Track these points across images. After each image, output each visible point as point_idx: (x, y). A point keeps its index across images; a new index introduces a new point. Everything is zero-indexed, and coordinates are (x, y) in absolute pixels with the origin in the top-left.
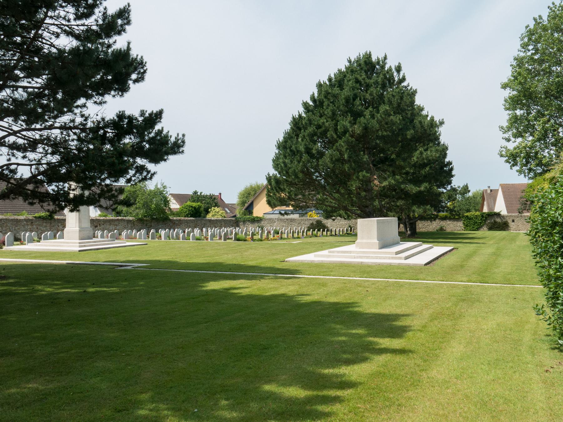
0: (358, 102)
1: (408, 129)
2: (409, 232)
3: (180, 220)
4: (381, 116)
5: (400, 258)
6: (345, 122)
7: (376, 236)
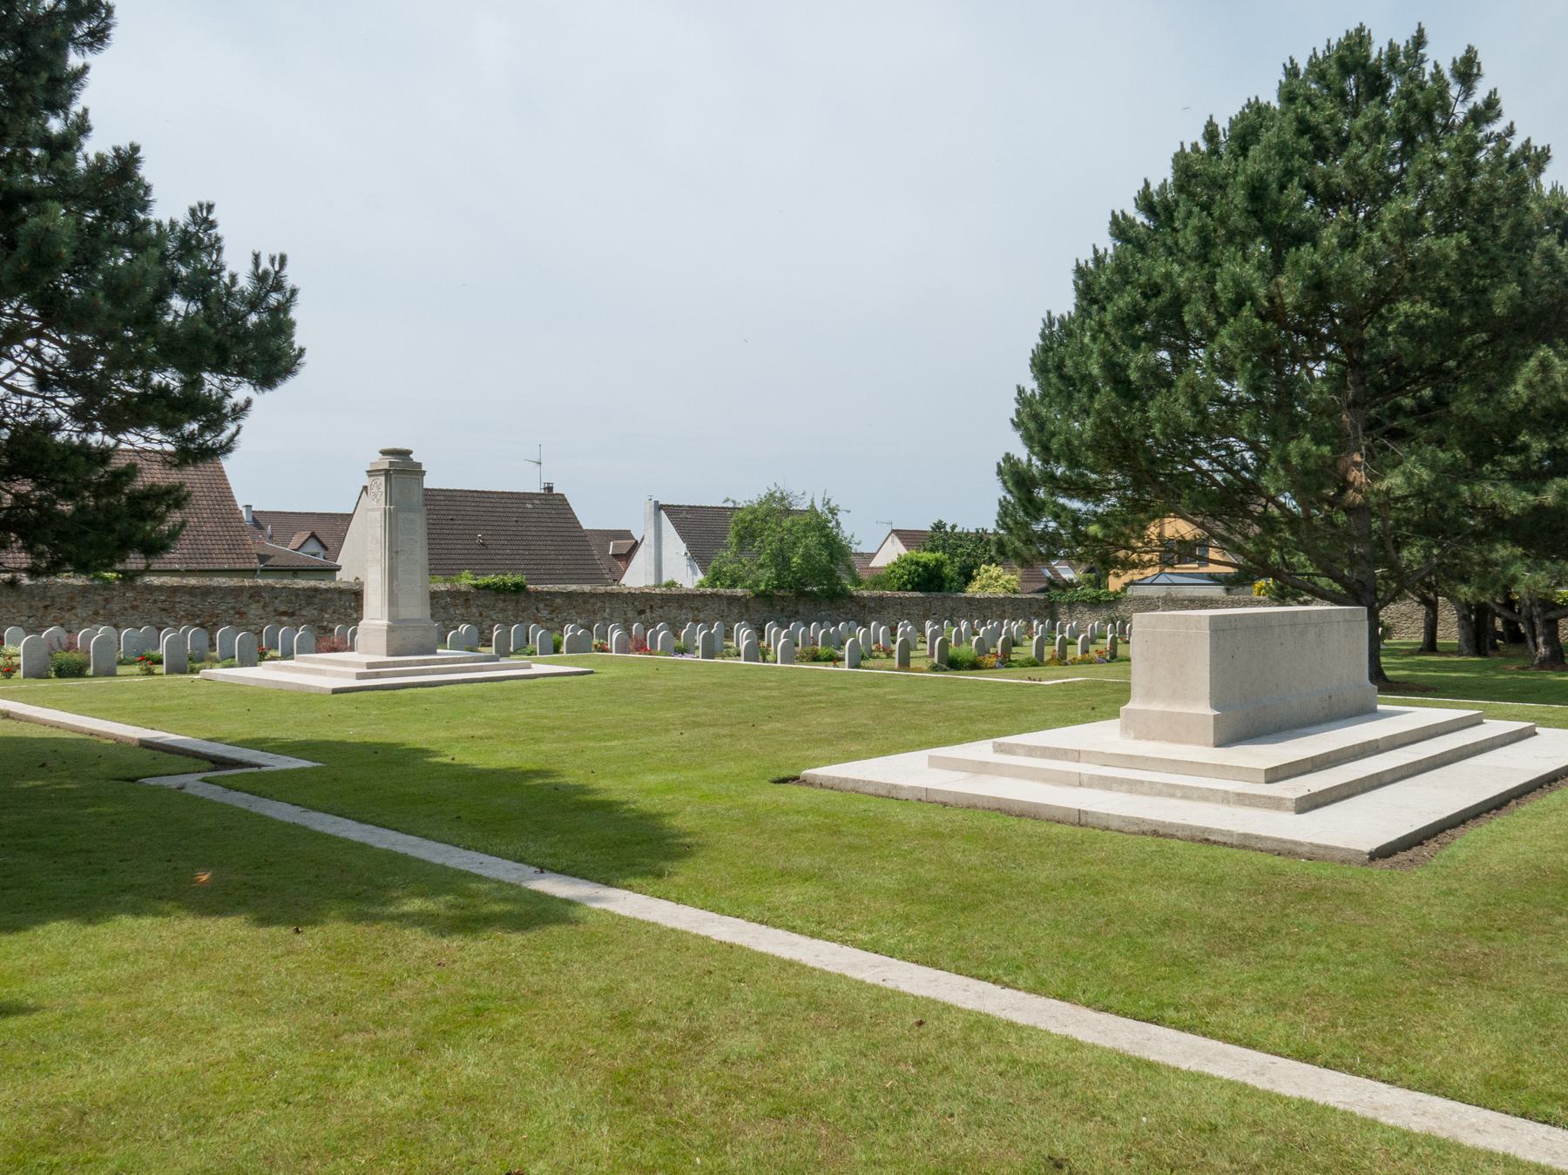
0: (1294, 192)
1: (1499, 277)
2: (1542, 650)
3: (881, 598)
4: (1384, 239)
5: (1276, 804)
6: (1241, 267)
7: (1205, 689)
